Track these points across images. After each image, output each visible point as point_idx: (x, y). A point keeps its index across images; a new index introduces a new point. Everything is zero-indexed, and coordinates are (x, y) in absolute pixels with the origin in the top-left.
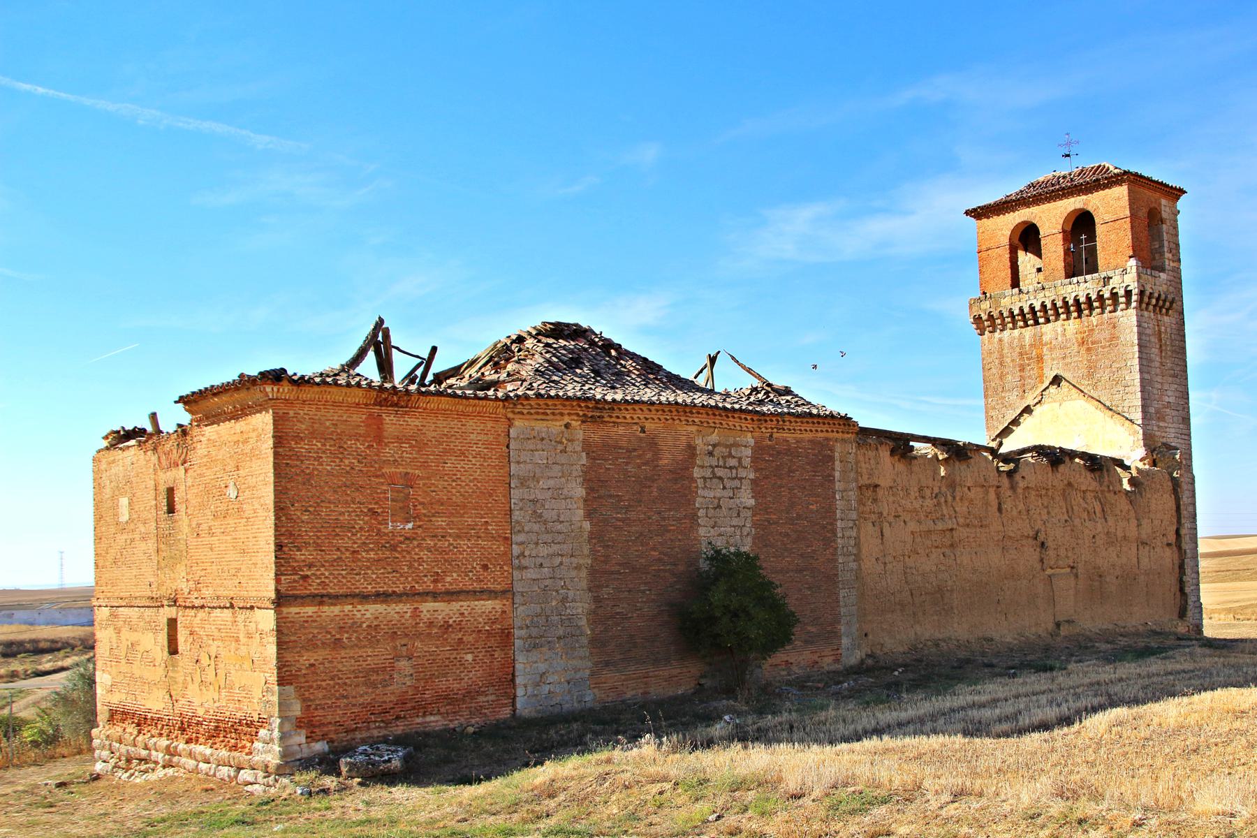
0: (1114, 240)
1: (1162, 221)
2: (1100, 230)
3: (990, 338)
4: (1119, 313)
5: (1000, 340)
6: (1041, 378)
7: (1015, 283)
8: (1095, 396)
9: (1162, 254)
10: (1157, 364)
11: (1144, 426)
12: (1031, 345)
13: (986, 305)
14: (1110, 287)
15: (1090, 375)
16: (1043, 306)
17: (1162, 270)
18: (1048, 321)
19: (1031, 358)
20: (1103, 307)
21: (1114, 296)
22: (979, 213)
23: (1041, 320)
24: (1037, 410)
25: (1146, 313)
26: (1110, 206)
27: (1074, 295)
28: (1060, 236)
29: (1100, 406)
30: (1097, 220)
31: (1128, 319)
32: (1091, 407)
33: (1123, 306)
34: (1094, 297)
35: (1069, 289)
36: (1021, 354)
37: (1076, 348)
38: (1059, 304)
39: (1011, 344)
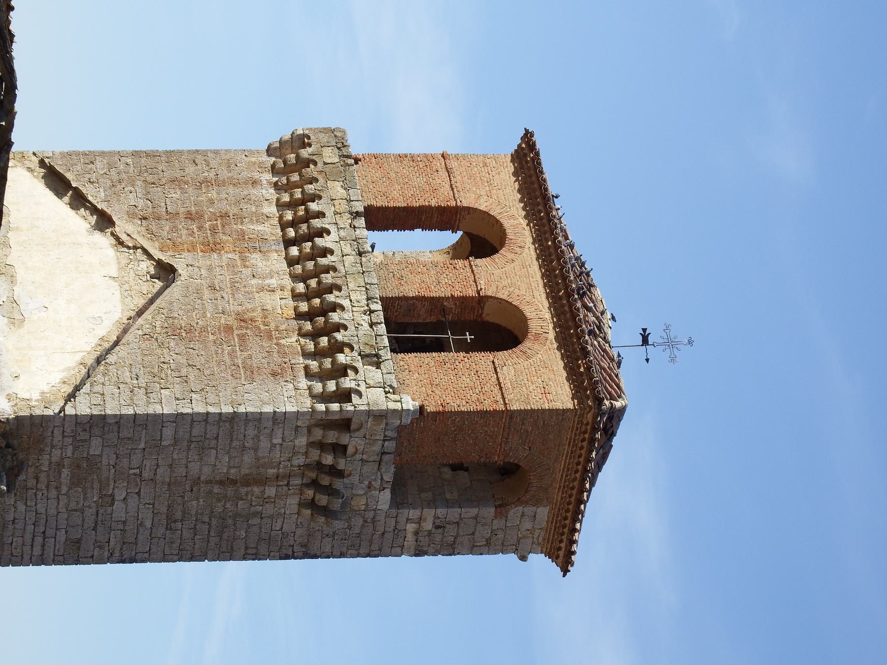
0: (453, 382)
1: (502, 508)
2: (483, 359)
3: (261, 165)
4: (303, 383)
5: (255, 183)
6: (176, 247)
7: (380, 218)
8: (129, 337)
9: (432, 503)
10: (194, 468)
11: (61, 418)
12: (243, 233)
13: (330, 155)
14: (359, 364)
15: (173, 331)
16: (326, 252)
17: (398, 502)
18: (291, 262)
19: (215, 231)
20: (318, 354)
21: (342, 371)
22: (527, 160)
23: (294, 251)
24: (104, 240)
25: (302, 441)
26: (535, 379)
27: (346, 303)
28: (471, 292)
29: (107, 345)
30: (502, 355)
31: (292, 397)
32: (107, 329)
33: (318, 387)
34: (339, 336)
35: (360, 297)
36: (224, 216)
37: (233, 307)
38: (327, 279)
39: (247, 199)
